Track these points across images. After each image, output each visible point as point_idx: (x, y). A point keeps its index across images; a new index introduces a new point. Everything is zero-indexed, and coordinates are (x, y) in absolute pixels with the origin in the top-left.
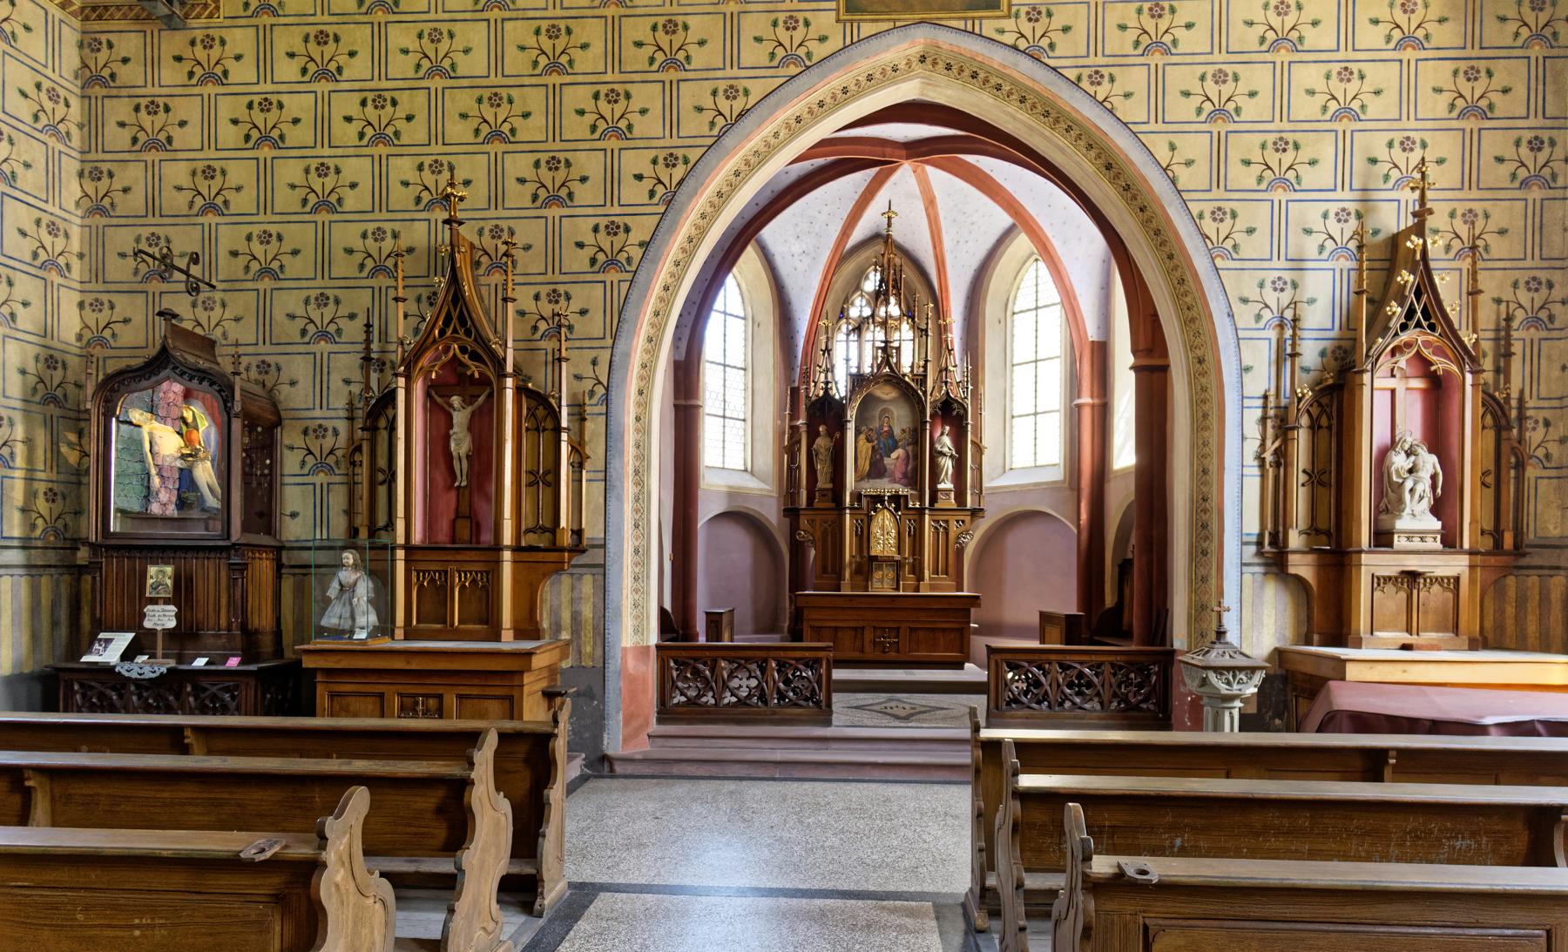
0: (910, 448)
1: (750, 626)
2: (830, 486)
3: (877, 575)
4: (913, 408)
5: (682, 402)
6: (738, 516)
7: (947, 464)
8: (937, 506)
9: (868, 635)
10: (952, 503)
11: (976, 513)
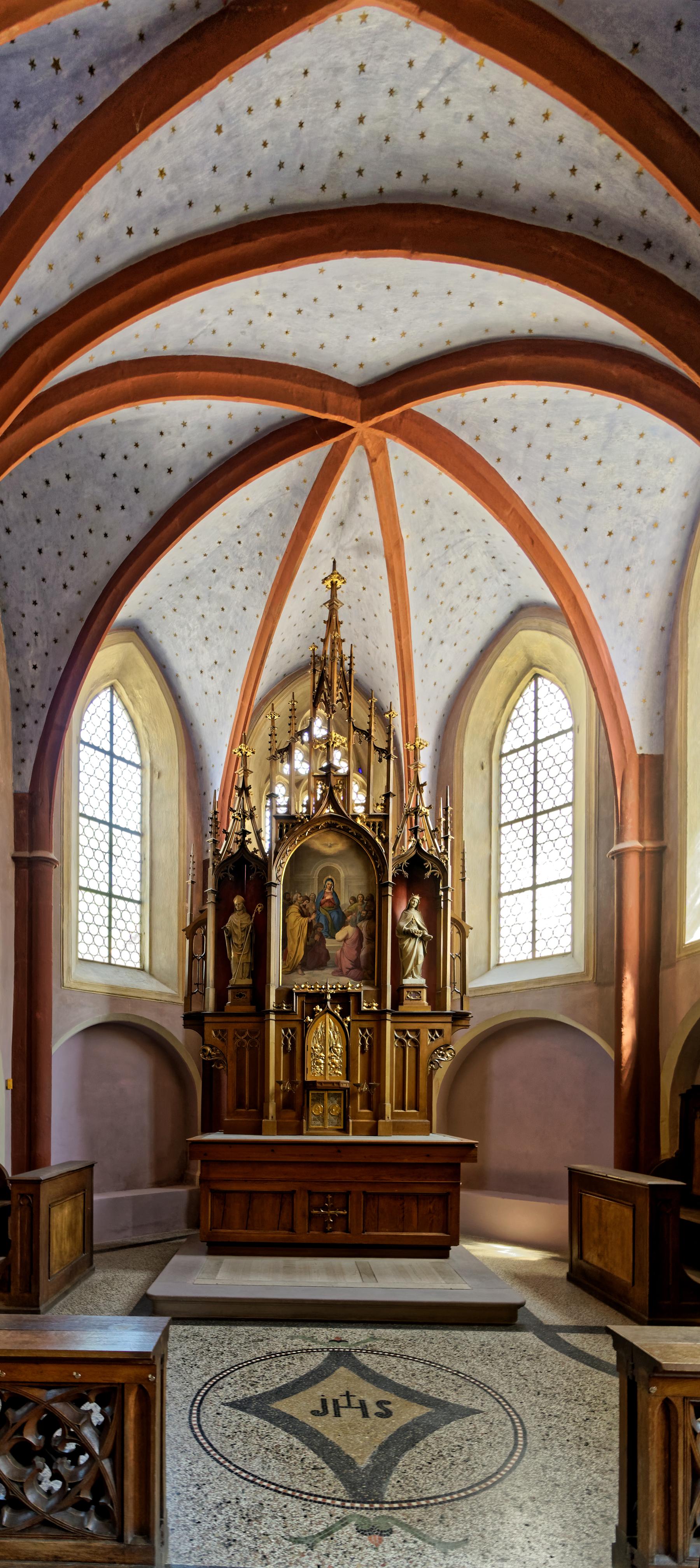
0: (363, 925)
1: (147, 1176)
2: (248, 982)
3: (316, 1110)
4: (367, 867)
5: (26, 854)
6: (123, 1027)
7: (417, 949)
8: (402, 1009)
9: (301, 1204)
10: (424, 1005)
11: (459, 1018)
